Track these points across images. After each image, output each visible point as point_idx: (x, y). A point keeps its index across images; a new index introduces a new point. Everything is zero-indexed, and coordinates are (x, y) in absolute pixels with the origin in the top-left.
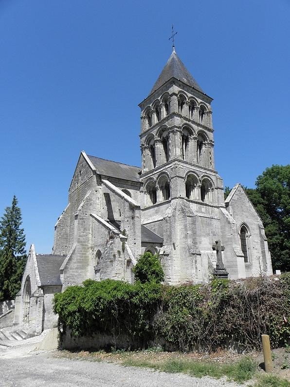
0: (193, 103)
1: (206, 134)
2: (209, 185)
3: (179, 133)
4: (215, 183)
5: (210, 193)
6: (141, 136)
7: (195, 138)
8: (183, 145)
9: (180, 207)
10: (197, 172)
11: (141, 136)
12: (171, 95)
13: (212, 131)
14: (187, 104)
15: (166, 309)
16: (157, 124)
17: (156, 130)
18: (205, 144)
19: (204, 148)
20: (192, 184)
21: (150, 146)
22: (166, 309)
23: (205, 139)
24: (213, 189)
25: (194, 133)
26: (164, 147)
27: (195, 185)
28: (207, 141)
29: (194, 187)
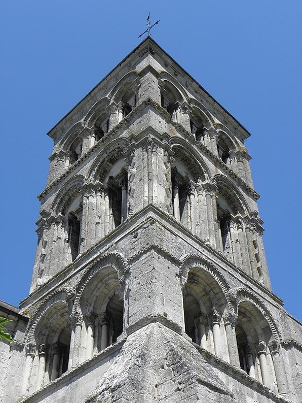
0: (200, 120)
1: (243, 199)
2: (260, 332)
3: (162, 150)
4: (280, 329)
5: (266, 360)
6: (42, 198)
7: (209, 188)
8: (173, 197)
9: (164, 353)
10: (222, 272)
11: (42, 198)
12: (143, 73)
13: (255, 197)
14: (185, 109)
15: (177, 274)
16: (96, 147)
17: (89, 165)
18: (237, 221)
19: (234, 230)
20: (204, 310)
21: (67, 217)
22: (177, 274)
23: (237, 208)
24: (275, 345)
25: (206, 175)
26: (112, 205)
27: (216, 313)
28: (243, 213)
29: (210, 322)
